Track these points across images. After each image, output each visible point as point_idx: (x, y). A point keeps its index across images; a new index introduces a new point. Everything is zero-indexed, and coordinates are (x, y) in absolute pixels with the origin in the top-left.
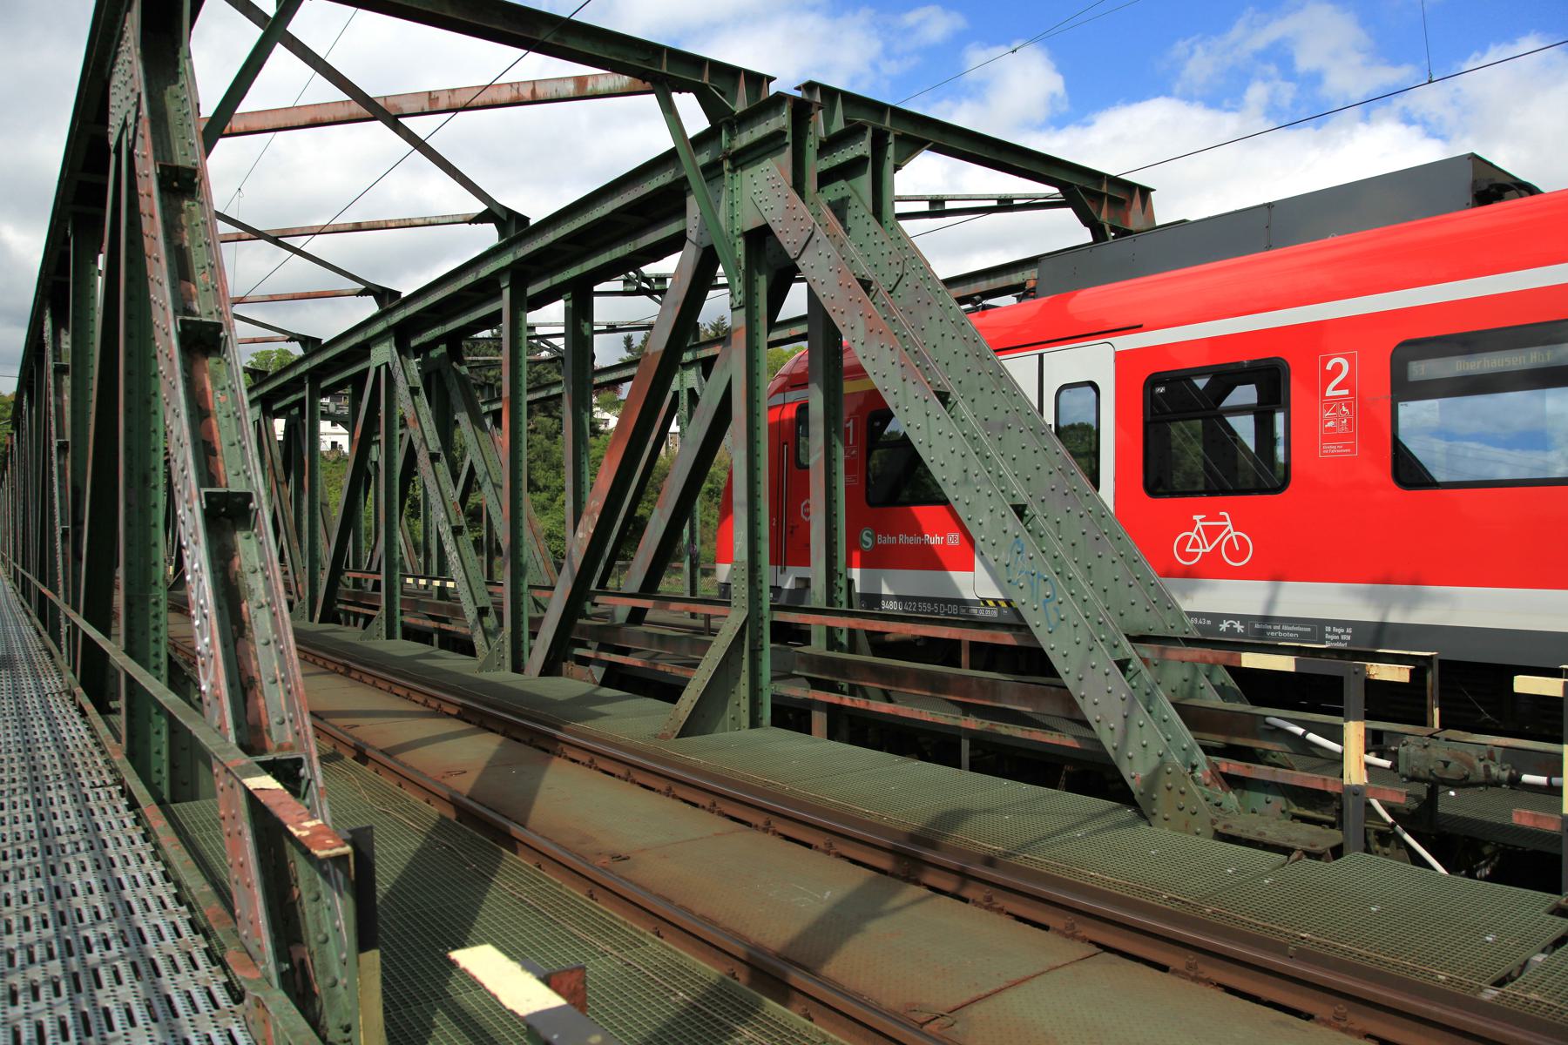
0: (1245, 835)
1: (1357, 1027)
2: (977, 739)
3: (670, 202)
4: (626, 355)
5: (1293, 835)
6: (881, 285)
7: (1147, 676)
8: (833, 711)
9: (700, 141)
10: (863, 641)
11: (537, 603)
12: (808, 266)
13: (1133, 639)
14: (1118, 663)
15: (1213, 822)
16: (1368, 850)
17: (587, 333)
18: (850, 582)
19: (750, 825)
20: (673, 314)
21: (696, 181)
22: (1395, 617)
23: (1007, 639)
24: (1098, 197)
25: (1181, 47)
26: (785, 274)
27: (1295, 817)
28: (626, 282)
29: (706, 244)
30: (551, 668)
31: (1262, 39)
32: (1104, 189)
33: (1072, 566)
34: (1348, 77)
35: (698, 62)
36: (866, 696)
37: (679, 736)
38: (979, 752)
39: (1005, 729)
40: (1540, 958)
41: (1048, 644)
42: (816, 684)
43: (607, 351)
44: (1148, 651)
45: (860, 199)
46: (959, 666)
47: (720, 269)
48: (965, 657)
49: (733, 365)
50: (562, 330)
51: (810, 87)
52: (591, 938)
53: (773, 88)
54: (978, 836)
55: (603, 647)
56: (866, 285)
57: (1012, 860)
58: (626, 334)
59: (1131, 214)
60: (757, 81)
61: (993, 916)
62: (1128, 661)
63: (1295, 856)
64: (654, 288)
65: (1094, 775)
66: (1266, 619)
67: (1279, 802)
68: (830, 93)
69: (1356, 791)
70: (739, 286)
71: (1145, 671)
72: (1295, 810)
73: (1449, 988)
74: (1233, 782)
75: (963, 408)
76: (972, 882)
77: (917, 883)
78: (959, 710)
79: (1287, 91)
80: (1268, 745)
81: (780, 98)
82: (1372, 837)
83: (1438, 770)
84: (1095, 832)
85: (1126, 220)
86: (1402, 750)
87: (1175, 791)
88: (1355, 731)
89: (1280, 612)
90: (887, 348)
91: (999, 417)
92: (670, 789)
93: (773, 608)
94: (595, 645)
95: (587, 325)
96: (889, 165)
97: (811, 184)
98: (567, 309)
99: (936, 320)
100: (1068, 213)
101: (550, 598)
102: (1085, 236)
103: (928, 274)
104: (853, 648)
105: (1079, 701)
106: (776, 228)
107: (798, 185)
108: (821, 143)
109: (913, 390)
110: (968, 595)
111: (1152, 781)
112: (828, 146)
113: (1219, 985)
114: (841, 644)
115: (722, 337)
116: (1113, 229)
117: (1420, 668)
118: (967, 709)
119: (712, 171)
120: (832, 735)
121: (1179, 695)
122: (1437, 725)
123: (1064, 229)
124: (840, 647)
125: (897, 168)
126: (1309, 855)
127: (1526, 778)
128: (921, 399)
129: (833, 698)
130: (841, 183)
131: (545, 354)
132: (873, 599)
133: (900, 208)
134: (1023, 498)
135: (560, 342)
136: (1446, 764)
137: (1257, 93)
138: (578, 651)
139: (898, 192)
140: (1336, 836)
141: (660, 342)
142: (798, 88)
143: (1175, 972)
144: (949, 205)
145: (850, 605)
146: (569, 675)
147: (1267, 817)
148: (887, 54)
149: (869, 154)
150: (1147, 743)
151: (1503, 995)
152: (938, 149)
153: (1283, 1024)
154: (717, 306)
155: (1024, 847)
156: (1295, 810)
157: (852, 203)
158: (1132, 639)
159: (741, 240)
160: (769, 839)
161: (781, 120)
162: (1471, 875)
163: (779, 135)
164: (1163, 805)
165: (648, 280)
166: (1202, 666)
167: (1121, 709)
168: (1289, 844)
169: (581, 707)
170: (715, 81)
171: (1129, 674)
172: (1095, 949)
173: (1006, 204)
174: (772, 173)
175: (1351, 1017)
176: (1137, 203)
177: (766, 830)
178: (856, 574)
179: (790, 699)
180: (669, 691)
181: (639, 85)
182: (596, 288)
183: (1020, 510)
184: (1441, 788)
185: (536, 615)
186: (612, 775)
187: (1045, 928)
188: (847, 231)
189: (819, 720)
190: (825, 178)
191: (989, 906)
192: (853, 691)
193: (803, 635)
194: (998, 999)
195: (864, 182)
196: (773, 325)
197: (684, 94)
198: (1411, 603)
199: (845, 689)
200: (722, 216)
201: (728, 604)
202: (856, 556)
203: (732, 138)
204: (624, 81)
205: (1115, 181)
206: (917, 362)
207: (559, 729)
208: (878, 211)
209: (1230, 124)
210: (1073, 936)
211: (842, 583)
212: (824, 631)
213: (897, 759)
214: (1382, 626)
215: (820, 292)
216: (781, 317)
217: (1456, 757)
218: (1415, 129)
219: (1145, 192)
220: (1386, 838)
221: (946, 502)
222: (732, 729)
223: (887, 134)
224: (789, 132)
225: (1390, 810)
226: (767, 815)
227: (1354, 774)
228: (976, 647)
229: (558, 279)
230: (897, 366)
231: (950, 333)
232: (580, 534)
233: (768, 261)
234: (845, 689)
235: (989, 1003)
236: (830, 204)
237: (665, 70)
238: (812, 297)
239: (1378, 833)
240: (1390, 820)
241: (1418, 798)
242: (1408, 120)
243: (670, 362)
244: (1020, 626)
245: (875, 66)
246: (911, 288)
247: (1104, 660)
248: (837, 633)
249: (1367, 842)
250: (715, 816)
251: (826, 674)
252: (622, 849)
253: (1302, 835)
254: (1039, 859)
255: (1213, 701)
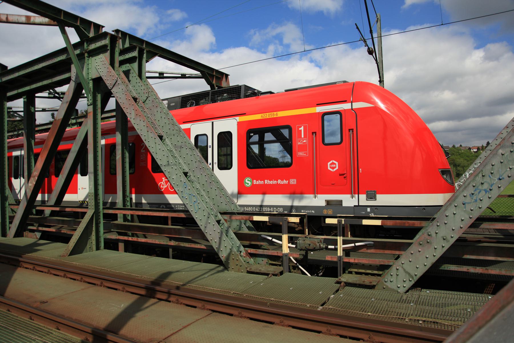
0: (255, 271)
1: (286, 324)
2: (174, 248)
3: (64, 66)
4: (52, 120)
5: (269, 270)
6: (141, 99)
7: (226, 225)
8: (126, 242)
9: (76, 46)
10: (136, 218)
11: (13, 211)
12: (115, 92)
13: (221, 214)
14: (217, 221)
15: (246, 268)
16: (290, 272)
17: (33, 111)
18: (131, 199)
19: (95, 284)
20: (66, 106)
21: (74, 59)
22: (296, 203)
23: (183, 215)
24: (212, 76)
25: (252, 31)
26: (107, 95)
27: (270, 264)
28: (49, 94)
29: (78, 82)
30: (19, 234)
31: (274, 33)
32: (214, 74)
33: (202, 191)
34: (297, 47)
35: (76, 18)
36: (138, 237)
37: (69, 255)
38: (176, 252)
39: (183, 244)
40: (332, 296)
41: (195, 216)
42: (120, 234)
43: (41, 118)
44: (226, 217)
45: (134, 71)
46: (168, 225)
47: (84, 91)
48: (170, 222)
49: (88, 125)
50: (22, 109)
51: (117, 31)
52: (30, 335)
53: (104, 30)
54: (173, 281)
55: (40, 225)
56: (135, 99)
57: (187, 287)
58: (52, 112)
59: (223, 82)
60: (98, 27)
61: (179, 306)
62: (220, 220)
63: (270, 276)
64: (59, 96)
65: (210, 256)
66: (261, 206)
67: (265, 260)
68: (124, 35)
69: (286, 255)
70: (90, 97)
71: (225, 223)
72: (270, 262)
73: (310, 308)
74: (252, 255)
75: (167, 141)
76: (172, 295)
77: (154, 298)
78: (168, 239)
79: (280, 49)
80: (262, 243)
81: (106, 34)
82: (291, 268)
83: (307, 246)
84: (211, 275)
85: (221, 84)
86: (298, 242)
87: (235, 260)
88: (285, 237)
89: (265, 204)
90: (142, 121)
91: (179, 144)
92: (65, 275)
93: (103, 208)
94: (37, 225)
95: (33, 108)
96: (144, 60)
97: (117, 64)
98: (24, 102)
99: (159, 112)
100: (203, 80)
101: (18, 208)
102: (208, 88)
103: (157, 98)
104: (132, 220)
105: (205, 234)
106: (104, 78)
107: (112, 64)
108: (120, 50)
109: (151, 135)
110: (171, 202)
111: (228, 258)
112: (123, 52)
113: (248, 318)
114: (128, 220)
115: (85, 116)
116: (217, 86)
117: (302, 217)
118: (171, 239)
119: (81, 57)
120: (126, 251)
121: (236, 230)
122: (307, 234)
123: (201, 86)
124: (128, 221)
125: (147, 61)
126: (274, 275)
127: (330, 247)
128: (153, 138)
129: (126, 238)
130: (128, 65)
131: (18, 118)
132: (139, 204)
133: (148, 75)
134: (187, 170)
135: (22, 114)
136: (310, 245)
137: (271, 48)
138: (30, 227)
139: (147, 69)
140: (281, 269)
141: (60, 115)
142: (113, 31)
143: (235, 316)
144: (165, 75)
145: (131, 206)
146: (26, 237)
147: (263, 265)
148: (161, 22)
149: (137, 56)
150: (227, 245)
151: (323, 308)
152: (161, 56)
153: (266, 326)
154: (82, 105)
155: (189, 282)
156: (270, 262)
157: (131, 72)
158: (221, 213)
159: (91, 81)
160: (102, 288)
161: (106, 41)
162: (318, 276)
163: (105, 46)
164: (231, 264)
165: (58, 93)
166: (243, 221)
167: (218, 235)
168: (268, 272)
169: (31, 248)
170: (83, 25)
171: (221, 225)
172: (211, 312)
173: (183, 76)
174: (103, 59)
175: (285, 321)
176: (224, 79)
177: (101, 286)
178: (133, 196)
179: (111, 239)
180: (66, 239)
181: (52, 22)
182: (37, 95)
183: (186, 174)
184: (309, 252)
185: (12, 215)
186: (42, 272)
187: (195, 307)
188: (129, 81)
189: (121, 246)
190: (122, 63)
191: (178, 302)
192: (133, 235)
193: (115, 217)
194: (180, 333)
195: (135, 65)
196: (103, 112)
197: (70, 28)
198: (301, 199)
199: (130, 235)
200: (85, 73)
201: (87, 208)
202: (133, 190)
203: (88, 46)
204: (46, 20)
205: (217, 71)
206: (152, 125)
207: (21, 257)
208: (140, 75)
209: (264, 56)
210: (204, 309)
211: (128, 199)
212: (122, 216)
213: (148, 257)
214: (292, 207)
215: (119, 101)
216: (106, 109)
217: (312, 242)
218: (313, 64)
219: (227, 76)
220: (295, 267)
221: (162, 172)
222: (90, 251)
223: (144, 50)
224: (109, 46)
225: (296, 259)
226: (101, 280)
227: (286, 250)
228: (173, 218)
229: (20, 90)
230: (145, 127)
231: (164, 116)
232: (30, 185)
233: (101, 89)
234: (130, 235)
235: (177, 335)
236: (124, 72)
237: (62, 18)
238: (117, 103)
239: (293, 266)
240: (295, 262)
241: (303, 255)
242: (311, 61)
243: (65, 123)
244: (186, 211)
245: (156, 26)
246: (151, 101)
247: (213, 220)
248: (127, 216)
249: (289, 269)
250: (82, 283)
251: (123, 230)
252: (44, 299)
253: (272, 269)
254: (193, 286)
255: (245, 231)
